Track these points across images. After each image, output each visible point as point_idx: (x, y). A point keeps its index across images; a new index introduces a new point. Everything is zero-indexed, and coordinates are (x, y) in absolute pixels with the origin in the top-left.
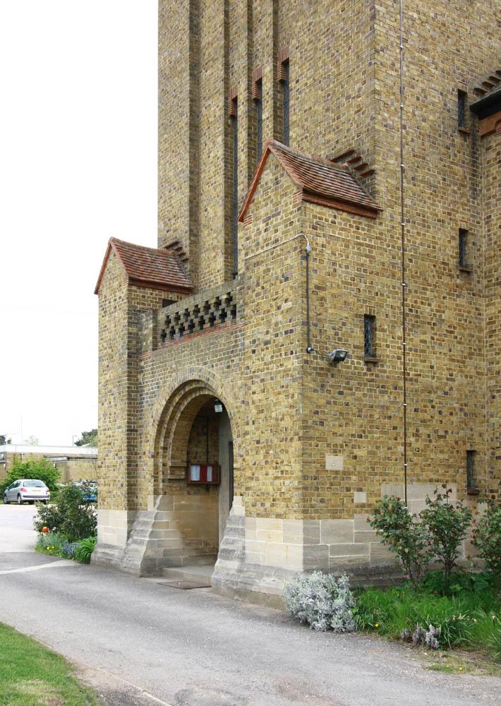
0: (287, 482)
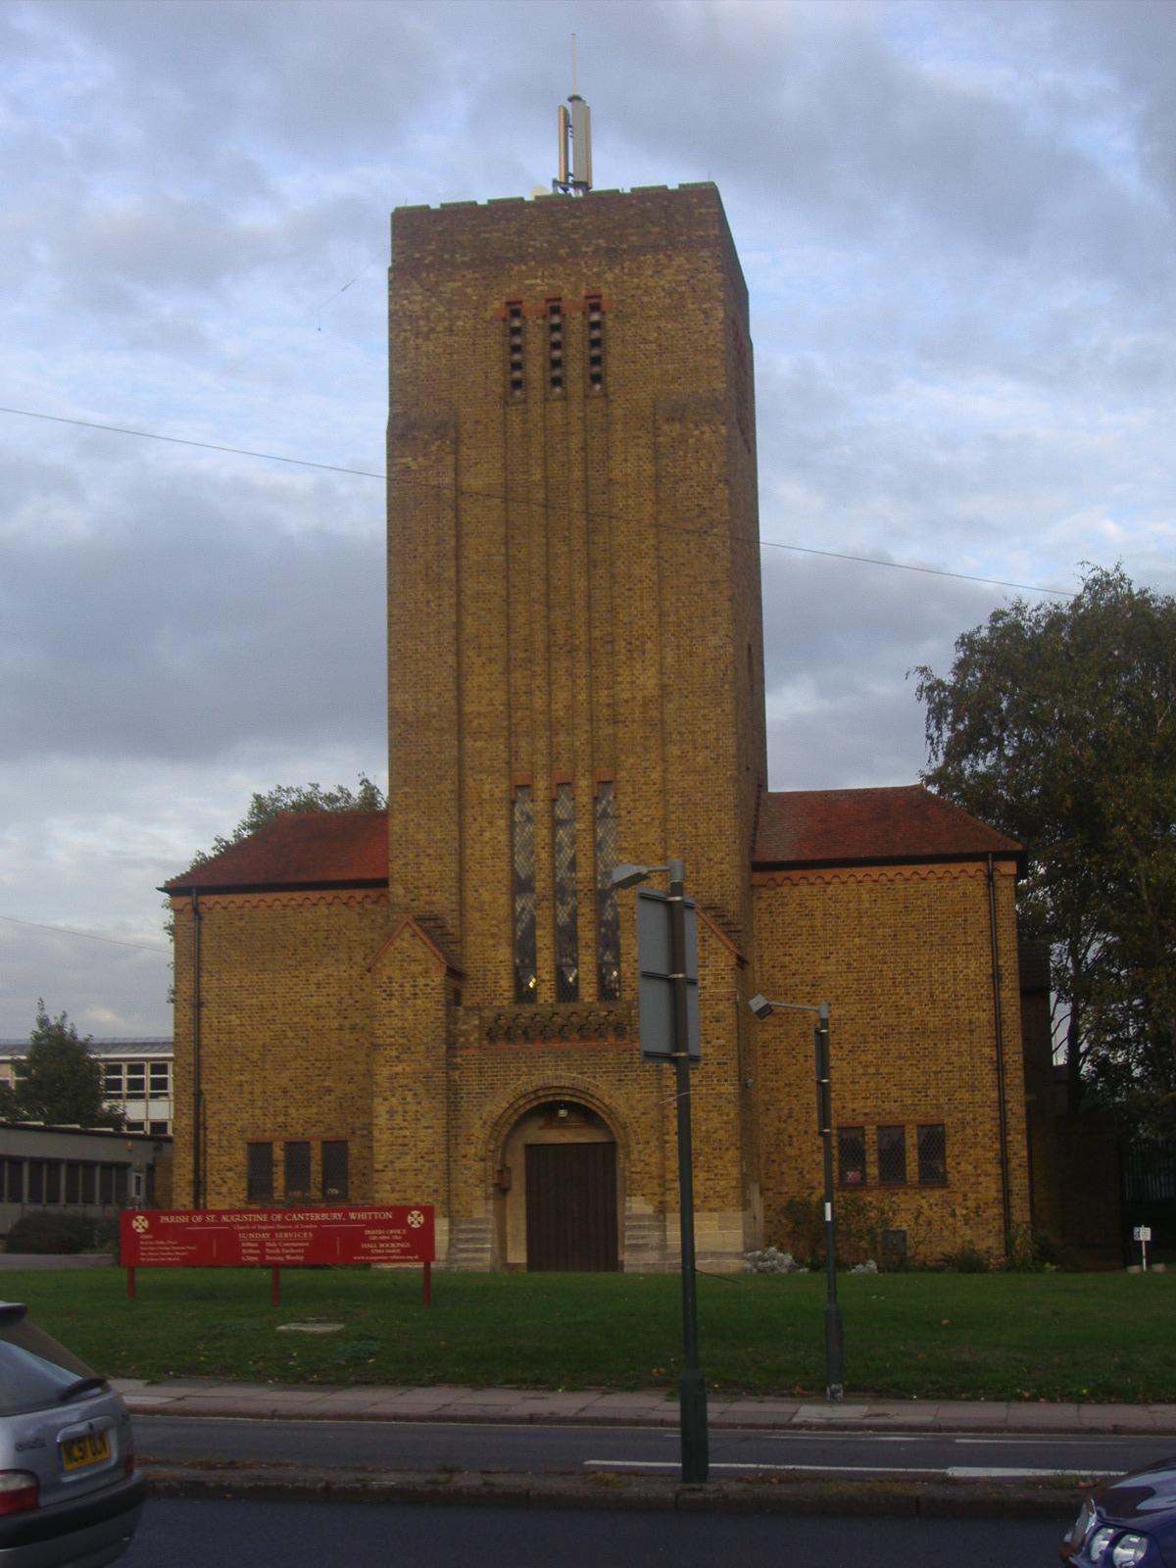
0: (722, 1183)
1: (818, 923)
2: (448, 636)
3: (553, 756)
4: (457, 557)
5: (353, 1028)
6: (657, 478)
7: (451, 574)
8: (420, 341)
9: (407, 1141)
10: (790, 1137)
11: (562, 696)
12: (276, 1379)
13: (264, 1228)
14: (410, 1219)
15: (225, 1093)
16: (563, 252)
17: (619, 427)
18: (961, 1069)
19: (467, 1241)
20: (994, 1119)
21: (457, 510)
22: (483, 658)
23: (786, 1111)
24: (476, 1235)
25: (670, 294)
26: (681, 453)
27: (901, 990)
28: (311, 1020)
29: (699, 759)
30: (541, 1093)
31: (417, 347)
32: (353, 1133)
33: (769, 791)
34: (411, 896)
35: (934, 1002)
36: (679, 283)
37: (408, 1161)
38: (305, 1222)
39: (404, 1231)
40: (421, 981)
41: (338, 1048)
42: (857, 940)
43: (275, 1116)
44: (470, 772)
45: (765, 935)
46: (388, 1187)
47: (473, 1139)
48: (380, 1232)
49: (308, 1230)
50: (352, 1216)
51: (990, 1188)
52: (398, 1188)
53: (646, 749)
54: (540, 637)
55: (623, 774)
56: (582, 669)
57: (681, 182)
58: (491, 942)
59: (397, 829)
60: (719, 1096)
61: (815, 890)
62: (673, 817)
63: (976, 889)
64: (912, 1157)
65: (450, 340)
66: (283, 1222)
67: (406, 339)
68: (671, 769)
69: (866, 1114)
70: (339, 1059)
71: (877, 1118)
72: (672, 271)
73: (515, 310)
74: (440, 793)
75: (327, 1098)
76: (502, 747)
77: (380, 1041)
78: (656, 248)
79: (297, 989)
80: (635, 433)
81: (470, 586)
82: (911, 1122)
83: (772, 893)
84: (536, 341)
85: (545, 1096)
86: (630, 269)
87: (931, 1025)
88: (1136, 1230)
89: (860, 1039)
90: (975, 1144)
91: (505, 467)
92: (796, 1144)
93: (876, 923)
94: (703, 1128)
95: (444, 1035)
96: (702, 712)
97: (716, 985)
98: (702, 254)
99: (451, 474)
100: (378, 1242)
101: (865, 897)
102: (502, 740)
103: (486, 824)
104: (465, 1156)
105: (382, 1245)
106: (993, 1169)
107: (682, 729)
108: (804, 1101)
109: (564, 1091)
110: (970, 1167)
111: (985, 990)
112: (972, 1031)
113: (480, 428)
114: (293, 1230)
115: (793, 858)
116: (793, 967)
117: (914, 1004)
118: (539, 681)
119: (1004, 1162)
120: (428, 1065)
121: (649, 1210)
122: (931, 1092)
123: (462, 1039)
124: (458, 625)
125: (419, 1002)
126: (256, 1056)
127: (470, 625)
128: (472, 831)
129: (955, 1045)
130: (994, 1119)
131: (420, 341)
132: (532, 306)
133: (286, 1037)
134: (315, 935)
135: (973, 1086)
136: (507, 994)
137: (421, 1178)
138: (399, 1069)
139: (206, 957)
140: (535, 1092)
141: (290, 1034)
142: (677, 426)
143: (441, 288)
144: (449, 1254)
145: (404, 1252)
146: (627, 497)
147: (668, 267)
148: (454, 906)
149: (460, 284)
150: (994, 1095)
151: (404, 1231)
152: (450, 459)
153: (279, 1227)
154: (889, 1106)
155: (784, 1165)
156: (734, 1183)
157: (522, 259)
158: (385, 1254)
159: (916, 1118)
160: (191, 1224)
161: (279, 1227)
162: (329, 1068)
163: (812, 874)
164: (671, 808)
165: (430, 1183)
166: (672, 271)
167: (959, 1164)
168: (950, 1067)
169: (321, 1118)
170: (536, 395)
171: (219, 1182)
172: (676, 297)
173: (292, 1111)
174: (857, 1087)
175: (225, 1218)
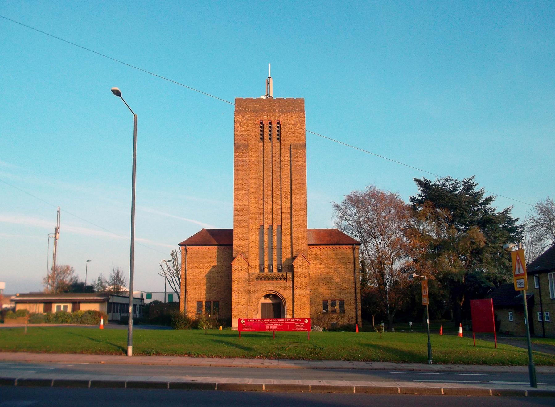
0: (306, 312)
5: (221, 276)
8: (241, 127)
9: (239, 302)
10: (313, 302)
12: (403, 362)
13: (272, 323)
14: (305, 321)
15: (192, 290)
18: (348, 289)
22: (254, 197)
23: (312, 297)
25: (294, 121)
26: (296, 156)
29: (300, 221)
31: (241, 129)
32: (220, 299)
34: (238, 248)
37: (239, 306)
38: (281, 322)
39: (304, 324)
40: (243, 267)
41: (218, 281)
42: (327, 261)
43: (203, 295)
47: (253, 302)
48: (298, 324)
49: (282, 323)
51: (353, 314)
52: (237, 312)
57: (297, 98)
58: (255, 259)
59: (235, 233)
60: (306, 293)
63: (351, 251)
65: (247, 128)
66: (276, 321)
69: (329, 298)
70: (217, 283)
71: (331, 299)
72: (295, 117)
74: (245, 226)
75: (215, 292)
78: (292, 111)
79: (209, 267)
80: (286, 151)
83: (310, 250)
84: (266, 129)
86: (286, 116)
89: (327, 282)
95: (248, 279)
96: (300, 211)
100: (298, 326)
101: (329, 252)
103: (254, 233)
104: (251, 305)
105: (299, 327)
106: (354, 310)
107: (296, 215)
109: (273, 291)
112: (350, 281)
113: (254, 147)
114: (278, 323)
115: (327, 243)
119: (356, 309)
120: (244, 285)
122: (342, 294)
123: (251, 280)
125: (242, 271)
126: (199, 282)
131: (241, 127)
136: (258, 270)
138: (238, 286)
139: (188, 260)
142: (296, 150)
143: (246, 116)
145: (304, 328)
147: (294, 116)
149: (250, 116)
150: (354, 294)
151: (304, 324)
153: (275, 322)
156: (308, 312)
157: (263, 111)
158: (299, 329)
161: (275, 322)
162: (215, 285)
163: (318, 247)
165: (244, 311)
166: (295, 117)
167: (347, 309)
168: (346, 288)
169: (213, 296)
171: (190, 310)
172: (295, 122)
175: (262, 320)
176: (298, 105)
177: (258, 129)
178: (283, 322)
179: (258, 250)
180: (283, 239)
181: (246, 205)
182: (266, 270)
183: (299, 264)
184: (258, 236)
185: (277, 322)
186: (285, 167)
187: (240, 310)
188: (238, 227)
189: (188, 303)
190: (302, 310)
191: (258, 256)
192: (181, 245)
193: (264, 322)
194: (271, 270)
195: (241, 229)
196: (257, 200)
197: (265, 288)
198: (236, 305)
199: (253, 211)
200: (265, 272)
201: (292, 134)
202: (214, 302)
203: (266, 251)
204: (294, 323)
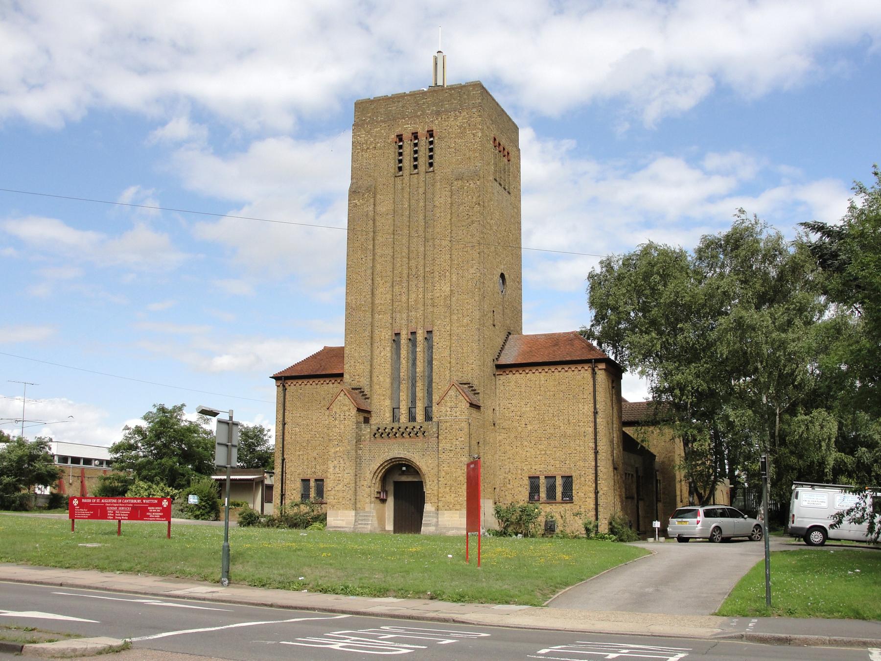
1: (523, 390)
2: (369, 272)
3: (408, 320)
4: (374, 240)
6: (451, 204)
7: (371, 247)
9: (340, 478)
11: (413, 296)
14: (163, 503)
16: (419, 113)
17: (438, 184)
19: (362, 520)
20: (593, 474)
21: (374, 220)
22: (383, 281)
24: (366, 518)
27: (556, 419)
28: (325, 430)
30: (393, 460)
33: (525, 332)
35: (569, 424)
36: (464, 123)
40: (347, 413)
42: (539, 397)
43: (312, 468)
44: (377, 328)
45: (501, 395)
46: (333, 497)
48: (153, 508)
50: (144, 501)
53: (445, 317)
54: (405, 272)
55: (436, 327)
56: (421, 284)
58: (383, 398)
59: (347, 352)
60: (461, 462)
61: (522, 375)
62: (454, 345)
64: (559, 490)
67: (358, 152)
68: (454, 325)
73: (400, 138)
76: (389, 317)
77: (331, 438)
81: (379, 251)
82: (559, 474)
83: (504, 377)
84: (408, 150)
85: (395, 461)
87: (568, 433)
88: (654, 522)
90: (585, 484)
91: (394, 202)
92: (511, 483)
93: (547, 390)
94: (454, 475)
97: (461, 415)
98: (473, 110)
99: (372, 206)
100: (152, 512)
101: (542, 378)
102: (389, 314)
106: (593, 495)
107: (458, 308)
108: (515, 465)
110: (583, 494)
111: (591, 419)
112: (585, 436)
113: (385, 187)
116: (513, 408)
117: (561, 424)
118: (405, 290)
121: (433, 509)
122: (567, 462)
124: (373, 267)
125: (346, 422)
126: (305, 444)
127: (379, 267)
128: (376, 352)
129: (578, 442)
130: (593, 474)
132: (407, 136)
133: (316, 437)
134: (328, 396)
135: (585, 459)
137: (345, 494)
138: (338, 449)
140: (391, 459)
141: (317, 436)
144: (355, 525)
145: (161, 517)
146: (441, 213)
147: (460, 117)
148: (368, 383)
150: (593, 463)
152: (372, 200)
153: (120, 505)
154: (550, 468)
155: (506, 492)
159: (561, 473)
160: (92, 503)
161: (120, 505)
164: (453, 341)
165: (348, 496)
170: (422, 174)
171: (290, 494)
173: (317, 466)
174: (537, 459)
176: (468, 95)
177: (392, 152)
178: (132, 503)
179: (388, 380)
180: (436, 357)
181: (368, 297)
182: (420, 417)
183: (449, 404)
184: (389, 355)
185: (124, 503)
186: (440, 216)
187: (341, 494)
188: (352, 340)
189: (287, 482)
190: (453, 495)
191: (389, 392)
192: (277, 378)
193: (105, 503)
194: (412, 418)
195: (358, 341)
196: (389, 285)
197: (388, 452)
198: (334, 485)
199: (382, 307)
200: (401, 421)
201: (455, 153)
202: (316, 480)
203: (404, 382)
204: (147, 507)
